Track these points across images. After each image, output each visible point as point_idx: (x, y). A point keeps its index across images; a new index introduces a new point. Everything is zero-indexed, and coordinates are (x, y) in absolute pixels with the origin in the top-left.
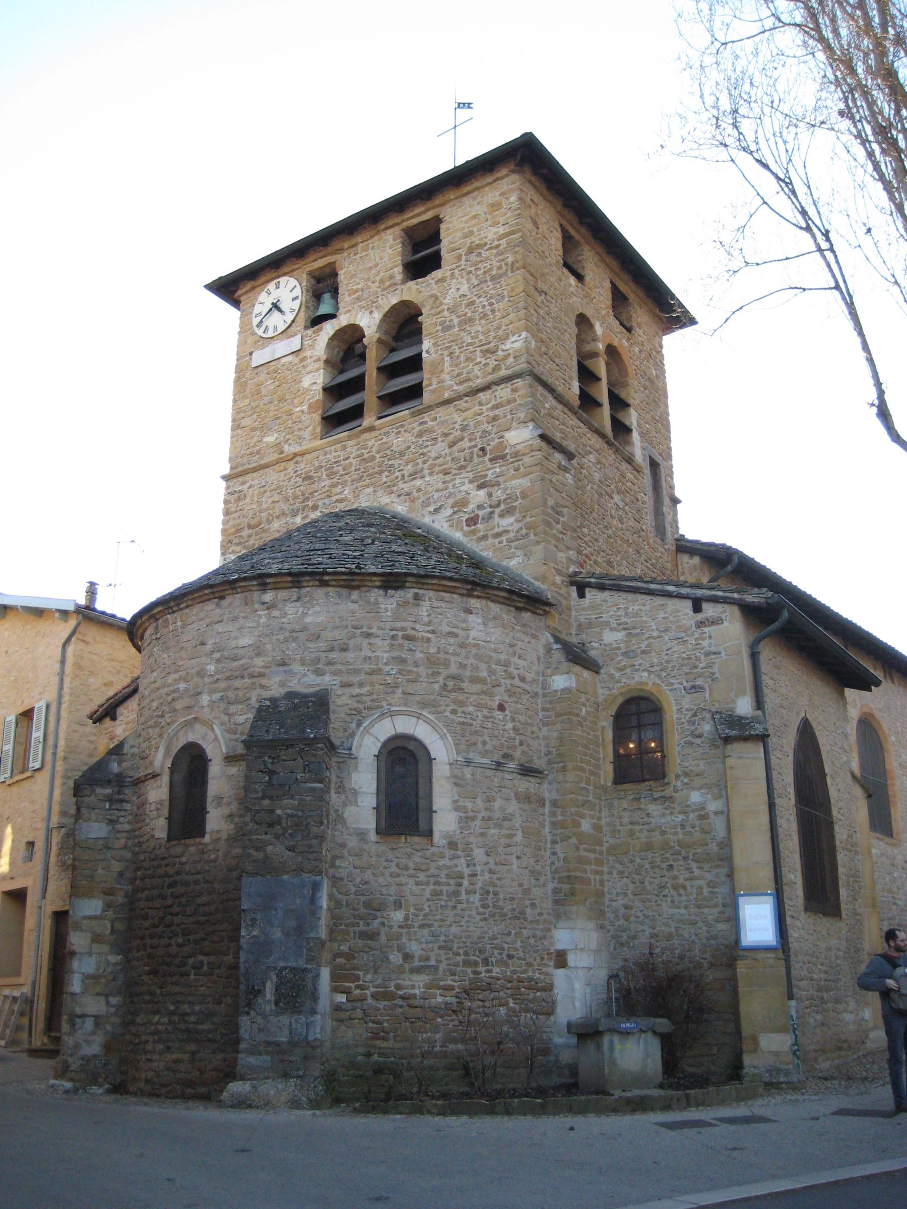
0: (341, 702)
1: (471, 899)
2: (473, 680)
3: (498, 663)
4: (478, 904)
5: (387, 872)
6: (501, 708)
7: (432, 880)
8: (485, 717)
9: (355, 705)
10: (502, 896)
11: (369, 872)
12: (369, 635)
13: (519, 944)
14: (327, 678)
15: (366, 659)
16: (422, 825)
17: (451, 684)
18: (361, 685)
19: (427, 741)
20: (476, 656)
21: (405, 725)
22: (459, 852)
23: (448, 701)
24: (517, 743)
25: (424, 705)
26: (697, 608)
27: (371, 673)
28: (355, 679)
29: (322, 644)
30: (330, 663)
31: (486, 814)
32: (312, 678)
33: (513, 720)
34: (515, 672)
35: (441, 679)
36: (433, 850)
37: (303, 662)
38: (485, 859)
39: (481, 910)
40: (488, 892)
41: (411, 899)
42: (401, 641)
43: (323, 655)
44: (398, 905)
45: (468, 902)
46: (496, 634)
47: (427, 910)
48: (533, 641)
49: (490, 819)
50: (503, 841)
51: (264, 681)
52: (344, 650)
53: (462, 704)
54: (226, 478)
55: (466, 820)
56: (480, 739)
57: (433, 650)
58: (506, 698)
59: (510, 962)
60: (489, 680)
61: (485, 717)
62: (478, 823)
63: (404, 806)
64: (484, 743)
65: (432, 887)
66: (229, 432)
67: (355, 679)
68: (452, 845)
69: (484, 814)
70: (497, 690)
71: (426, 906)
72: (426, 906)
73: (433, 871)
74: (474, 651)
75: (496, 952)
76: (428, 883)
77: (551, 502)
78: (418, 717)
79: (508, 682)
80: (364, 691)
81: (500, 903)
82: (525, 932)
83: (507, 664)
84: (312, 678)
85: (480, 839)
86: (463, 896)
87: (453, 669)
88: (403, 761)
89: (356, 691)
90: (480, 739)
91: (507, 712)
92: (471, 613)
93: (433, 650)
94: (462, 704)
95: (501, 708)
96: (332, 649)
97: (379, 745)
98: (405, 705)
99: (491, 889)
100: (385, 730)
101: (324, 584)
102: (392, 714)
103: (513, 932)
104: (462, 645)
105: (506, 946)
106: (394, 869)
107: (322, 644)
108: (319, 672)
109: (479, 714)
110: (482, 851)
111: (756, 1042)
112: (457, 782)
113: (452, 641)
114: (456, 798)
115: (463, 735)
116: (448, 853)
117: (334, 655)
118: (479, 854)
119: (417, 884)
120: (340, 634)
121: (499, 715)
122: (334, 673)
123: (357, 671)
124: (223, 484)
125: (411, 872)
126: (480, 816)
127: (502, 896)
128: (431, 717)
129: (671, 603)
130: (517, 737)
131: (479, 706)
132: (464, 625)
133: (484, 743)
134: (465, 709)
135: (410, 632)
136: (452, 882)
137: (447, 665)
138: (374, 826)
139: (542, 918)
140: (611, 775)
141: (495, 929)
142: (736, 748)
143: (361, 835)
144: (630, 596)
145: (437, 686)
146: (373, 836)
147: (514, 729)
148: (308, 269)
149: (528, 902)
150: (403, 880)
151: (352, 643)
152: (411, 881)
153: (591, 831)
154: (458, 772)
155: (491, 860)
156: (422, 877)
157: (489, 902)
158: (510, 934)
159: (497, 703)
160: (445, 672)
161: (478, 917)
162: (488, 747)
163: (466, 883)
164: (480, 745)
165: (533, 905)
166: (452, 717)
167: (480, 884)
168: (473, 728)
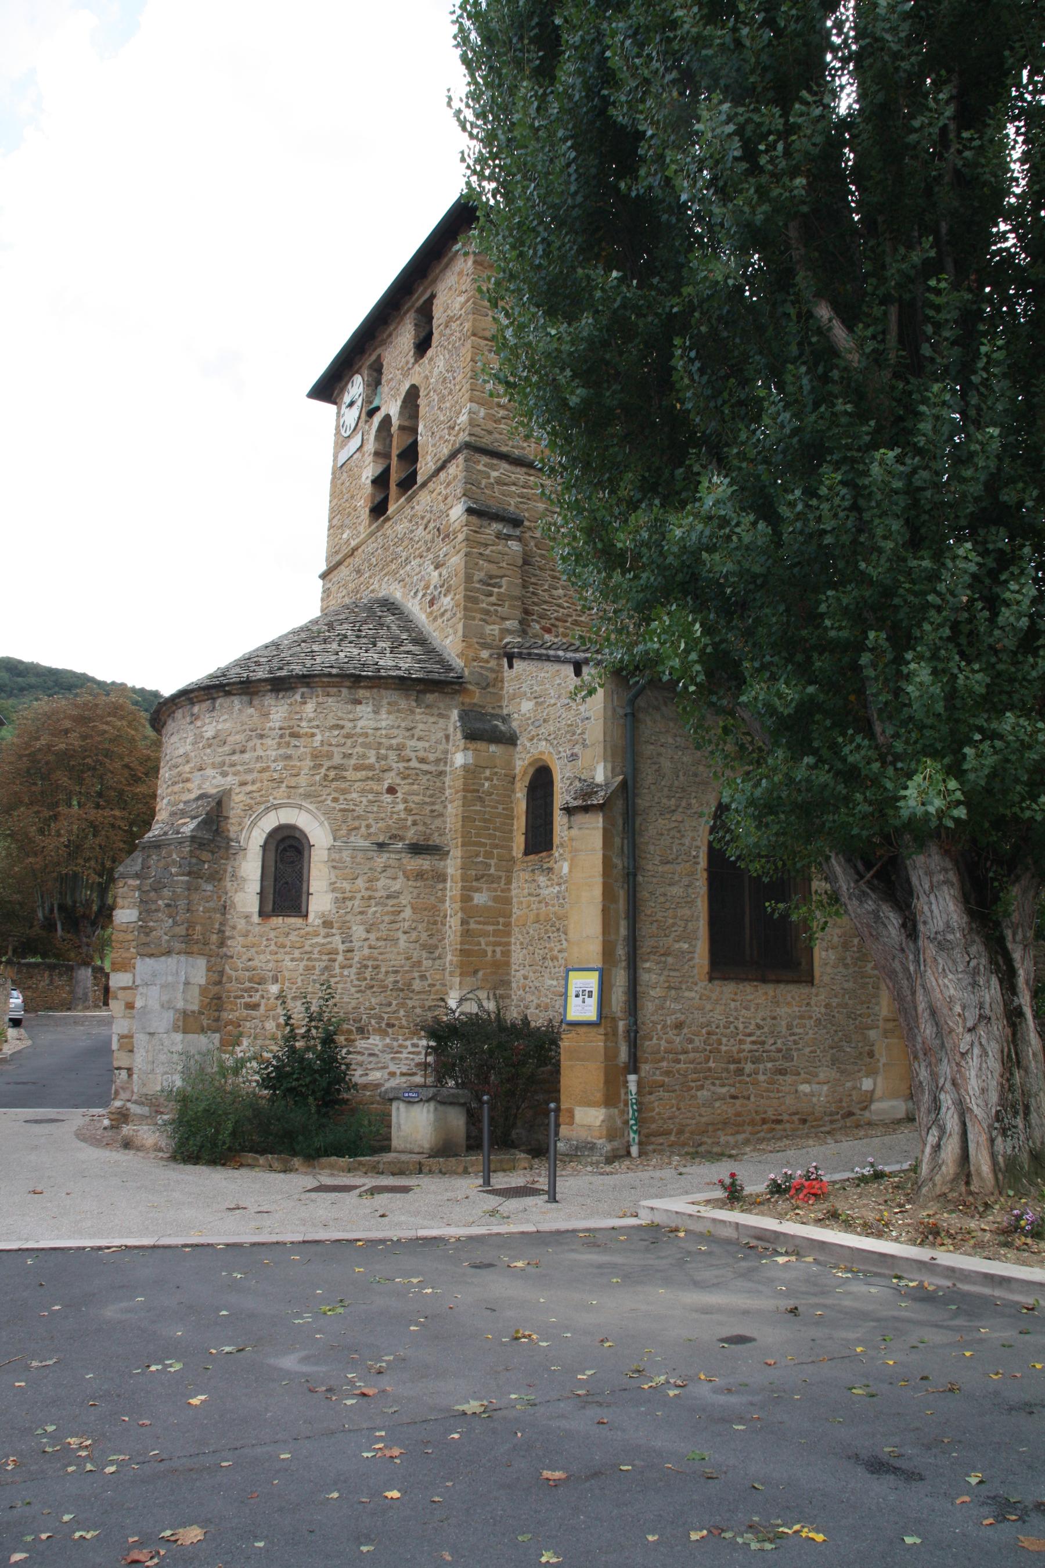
0: (238, 799)
1: (346, 973)
2: (357, 768)
3: (390, 748)
4: (353, 977)
5: (268, 950)
6: (391, 790)
7: (306, 956)
8: (369, 801)
9: (249, 801)
10: (383, 970)
11: (253, 950)
12: (262, 736)
13: (402, 1013)
14: (229, 778)
15: (259, 758)
16: (304, 909)
17: (332, 774)
18: (253, 782)
19: (307, 830)
20: (364, 745)
21: (286, 817)
22: (334, 931)
23: (328, 790)
24: (409, 823)
25: (307, 796)
26: (578, 673)
27: (263, 770)
28: (249, 778)
29: (227, 749)
30: (233, 765)
31: (367, 894)
32: (220, 780)
33: (405, 801)
34: (413, 755)
35: (323, 771)
36: (308, 929)
37: (214, 766)
38: (364, 935)
39: (356, 983)
40: (366, 967)
41: (287, 974)
42: (287, 739)
43: (227, 758)
44: (275, 980)
45: (342, 975)
46: (385, 720)
47: (300, 984)
48: (441, 721)
49: (370, 898)
50: (387, 919)
51: (189, 785)
52: (242, 752)
53: (344, 792)
54: (324, 576)
55: (341, 901)
56: (364, 823)
57: (317, 744)
58: (398, 781)
59: (390, 1030)
60: (377, 766)
61: (369, 801)
62: (357, 903)
63: (285, 891)
64: (368, 826)
65: (305, 962)
66: (326, 532)
67: (249, 778)
68: (327, 924)
69: (364, 893)
70: (387, 775)
71: (299, 980)
72: (299, 980)
73: (307, 948)
74: (360, 740)
75: (373, 1021)
76: (302, 959)
77: (479, 575)
78: (300, 807)
79: (401, 765)
80: (254, 788)
81: (381, 976)
82: (410, 1003)
83: (400, 748)
84: (220, 780)
85: (360, 917)
86: (337, 971)
87: (337, 760)
88: (288, 850)
89: (249, 788)
90: (364, 823)
91: (399, 794)
92: (360, 703)
93: (317, 744)
94: (344, 792)
95: (391, 790)
96: (234, 753)
97: (264, 836)
98: (289, 797)
99: (370, 963)
100: (270, 822)
101: (228, 694)
102: (276, 807)
103: (394, 1003)
104: (348, 736)
105: (386, 1016)
106: (273, 947)
107: (227, 749)
108: (224, 774)
109: (364, 799)
110: (362, 928)
111: (572, 1116)
112: (335, 865)
113: (336, 733)
114: (334, 880)
115: (344, 822)
116: (323, 931)
117: (235, 758)
118: (358, 931)
119: (292, 960)
120: (239, 738)
121: (388, 798)
122: (235, 774)
123: (250, 771)
124: (321, 582)
125: (288, 949)
126: (359, 896)
127: (383, 970)
128: (311, 807)
129: (551, 668)
130: (410, 818)
131: (363, 791)
132: (351, 716)
133: (368, 826)
134: (347, 796)
135: (296, 729)
136: (325, 957)
137: (330, 756)
138: (257, 909)
139: (434, 989)
140: (522, 847)
141: (373, 1000)
142: (580, 818)
143: (247, 917)
144: (539, 664)
145: (317, 778)
146: (256, 919)
147: (405, 809)
148: (368, 363)
149: (416, 975)
150: (279, 957)
151: (250, 744)
152: (287, 958)
153: (490, 903)
154: (337, 856)
155: (372, 936)
156: (297, 954)
157: (368, 975)
158: (390, 1004)
159: (386, 786)
160: (327, 764)
161: (353, 990)
162: (372, 830)
163: (340, 958)
164: (363, 829)
165: (423, 977)
166: (334, 805)
167: (356, 959)
168: (355, 814)
